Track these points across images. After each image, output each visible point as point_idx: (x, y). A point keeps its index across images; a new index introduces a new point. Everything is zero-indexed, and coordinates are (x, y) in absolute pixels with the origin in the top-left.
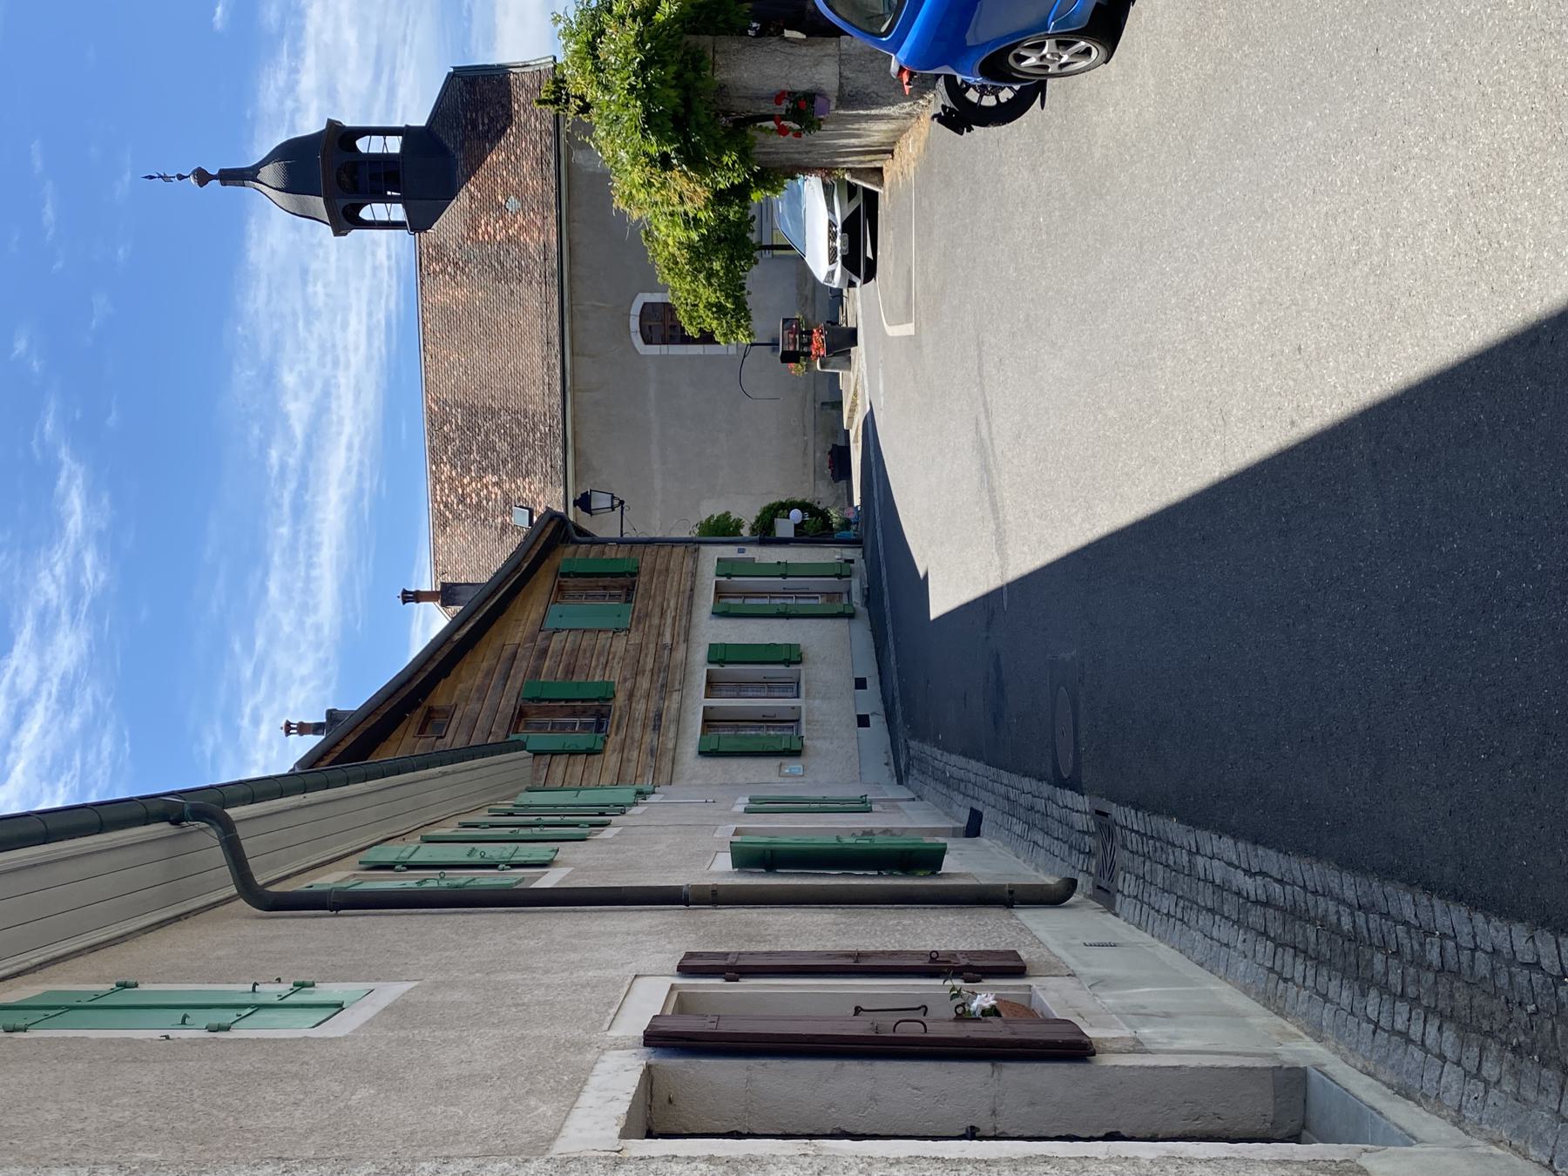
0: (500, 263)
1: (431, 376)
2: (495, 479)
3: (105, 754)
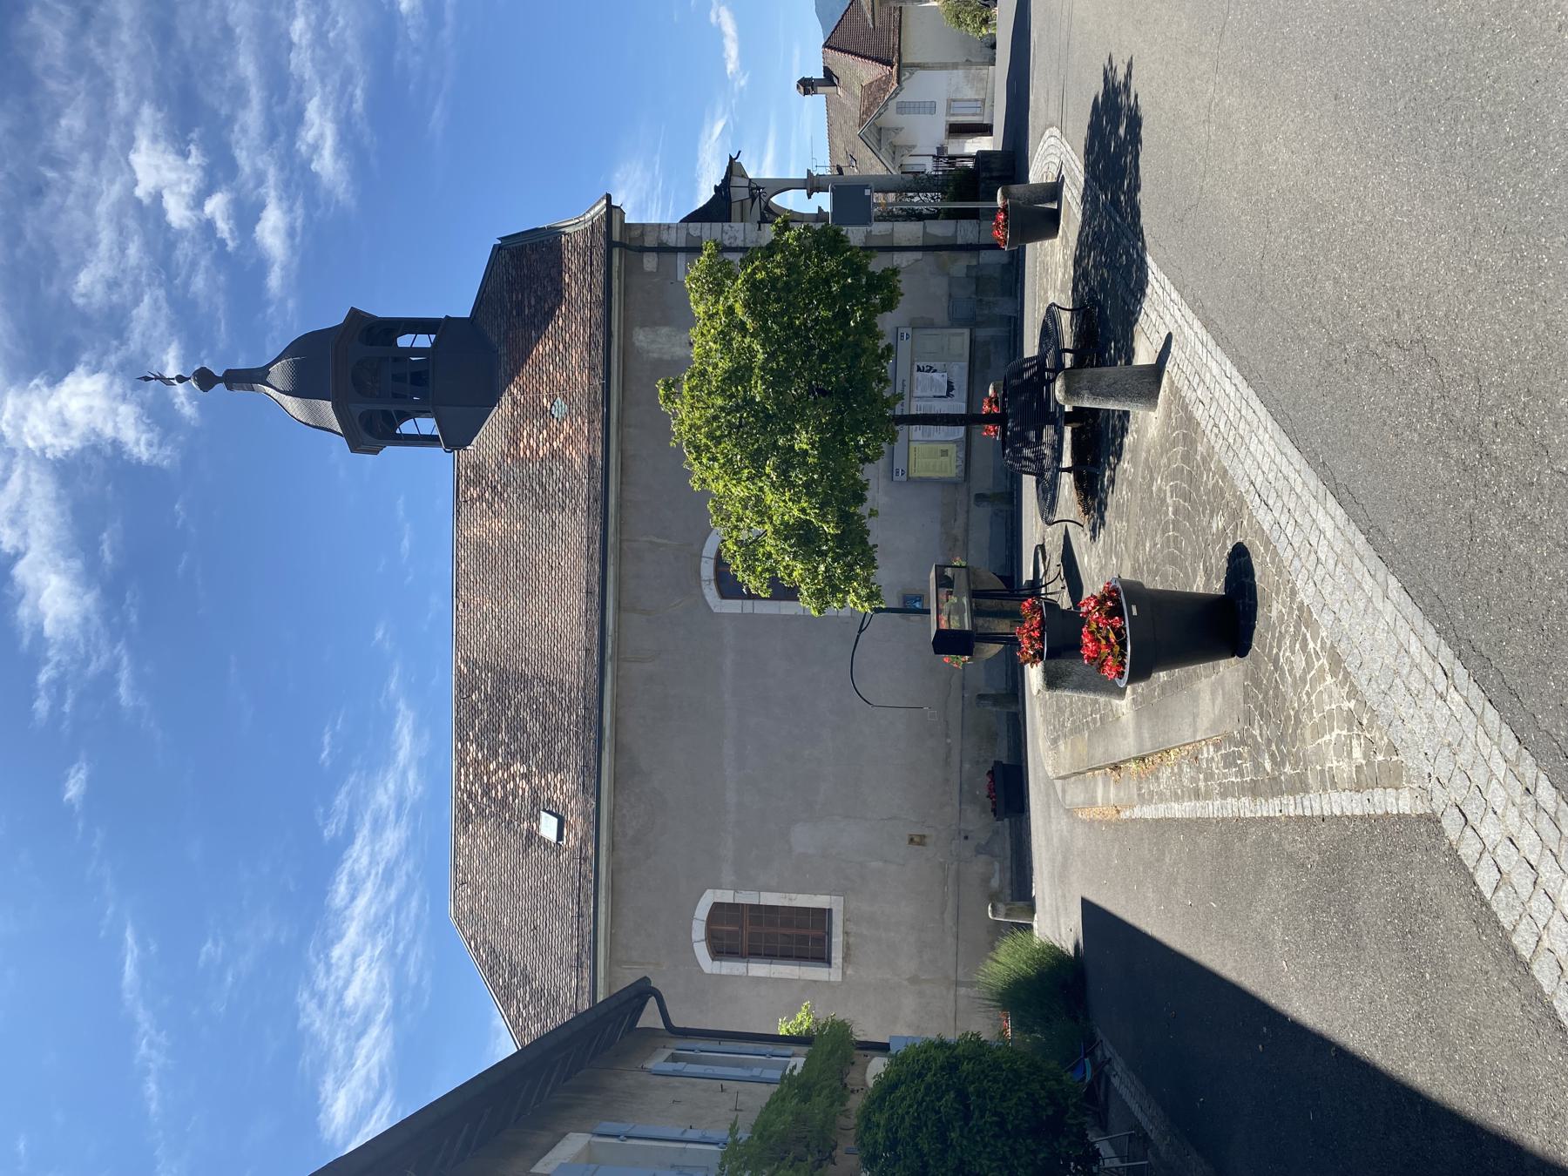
0: (541, 485)
1: (462, 629)
2: (523, 769)
3: (412, 915)
